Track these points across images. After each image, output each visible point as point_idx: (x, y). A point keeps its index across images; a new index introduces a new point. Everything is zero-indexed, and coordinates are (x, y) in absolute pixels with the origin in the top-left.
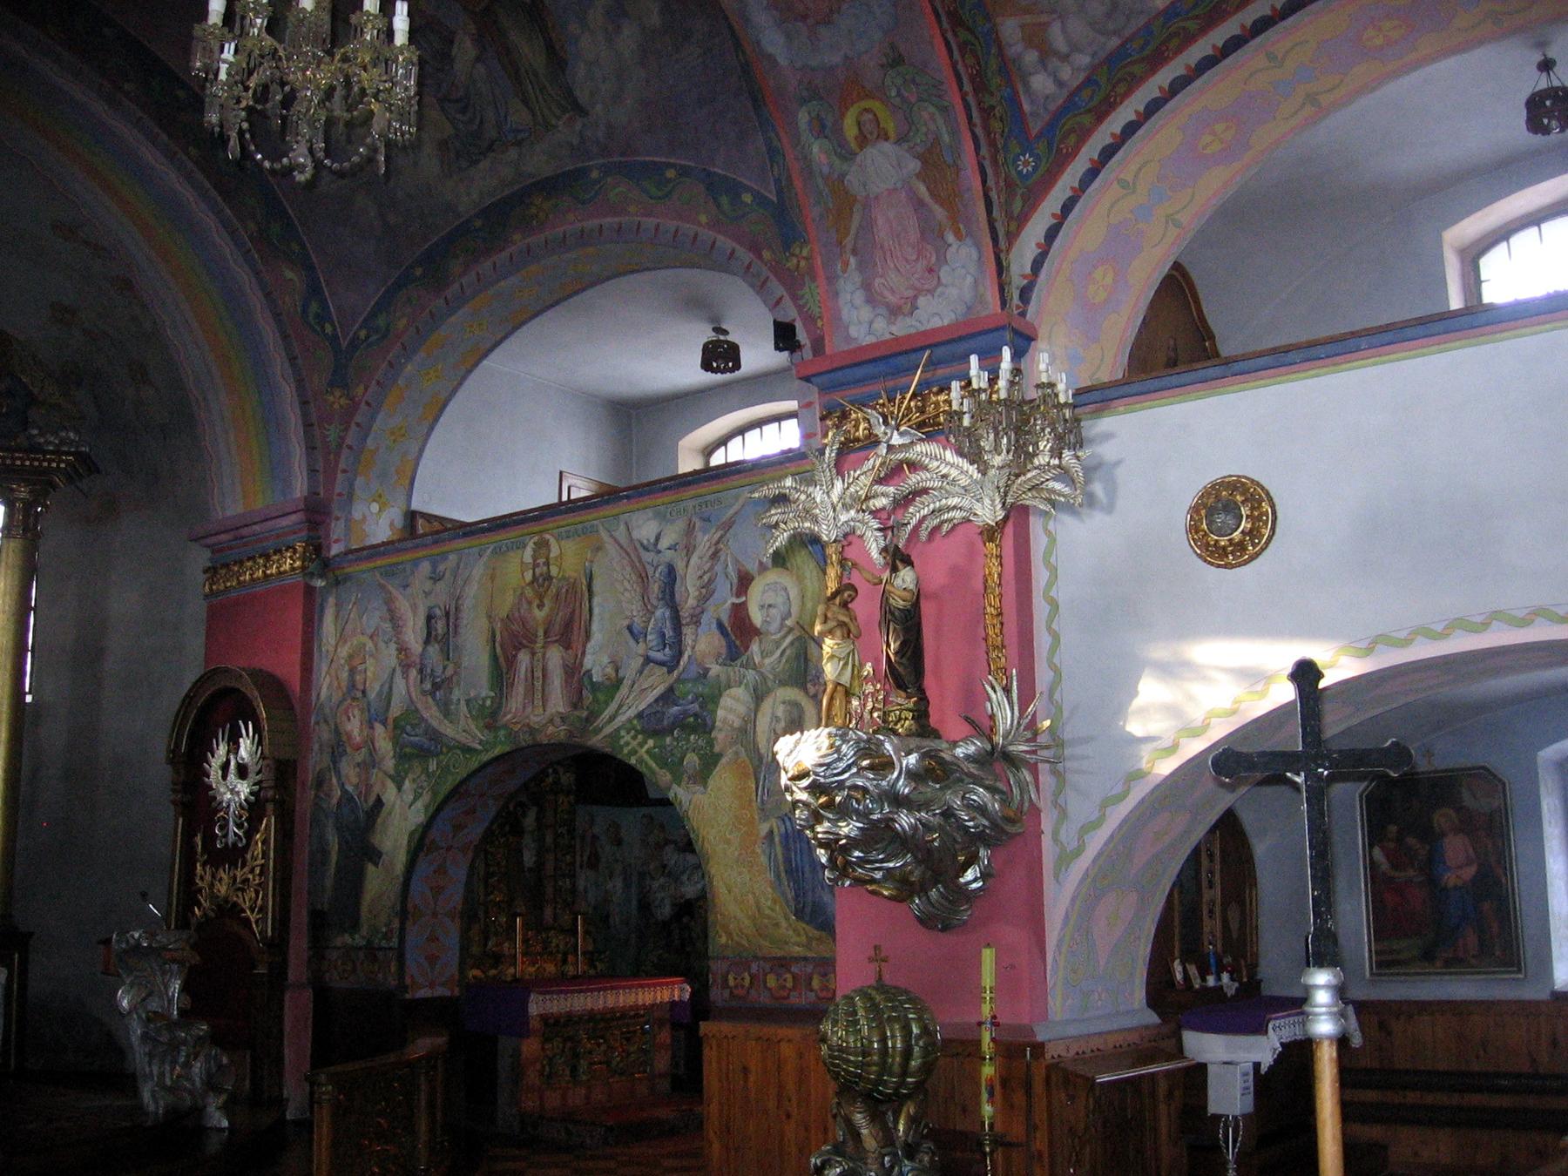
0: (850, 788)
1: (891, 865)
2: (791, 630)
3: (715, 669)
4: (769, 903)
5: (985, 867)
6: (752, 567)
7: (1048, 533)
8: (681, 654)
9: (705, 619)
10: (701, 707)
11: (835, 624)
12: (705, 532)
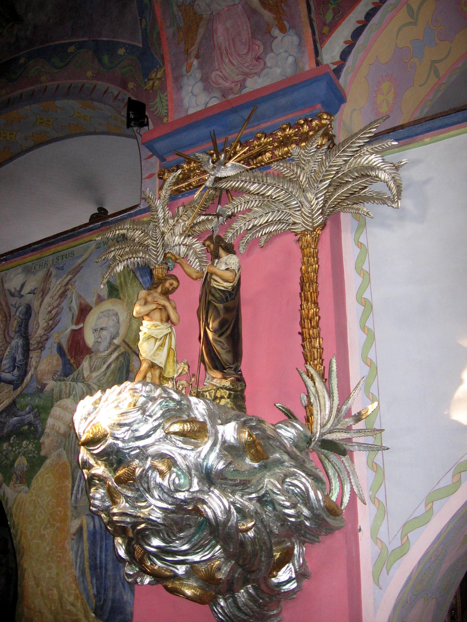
0: (154, 457)
1: (196, 558)
2: (117, 347)
3: (51, 384)
4: (72, 599)
5: (301, 567)
6: (91, 300)
7: (360, 245)
8: (26, 373)
9: (48, 345)
10: (35, 417)
11: (154, 306)
12: (57, 277)
